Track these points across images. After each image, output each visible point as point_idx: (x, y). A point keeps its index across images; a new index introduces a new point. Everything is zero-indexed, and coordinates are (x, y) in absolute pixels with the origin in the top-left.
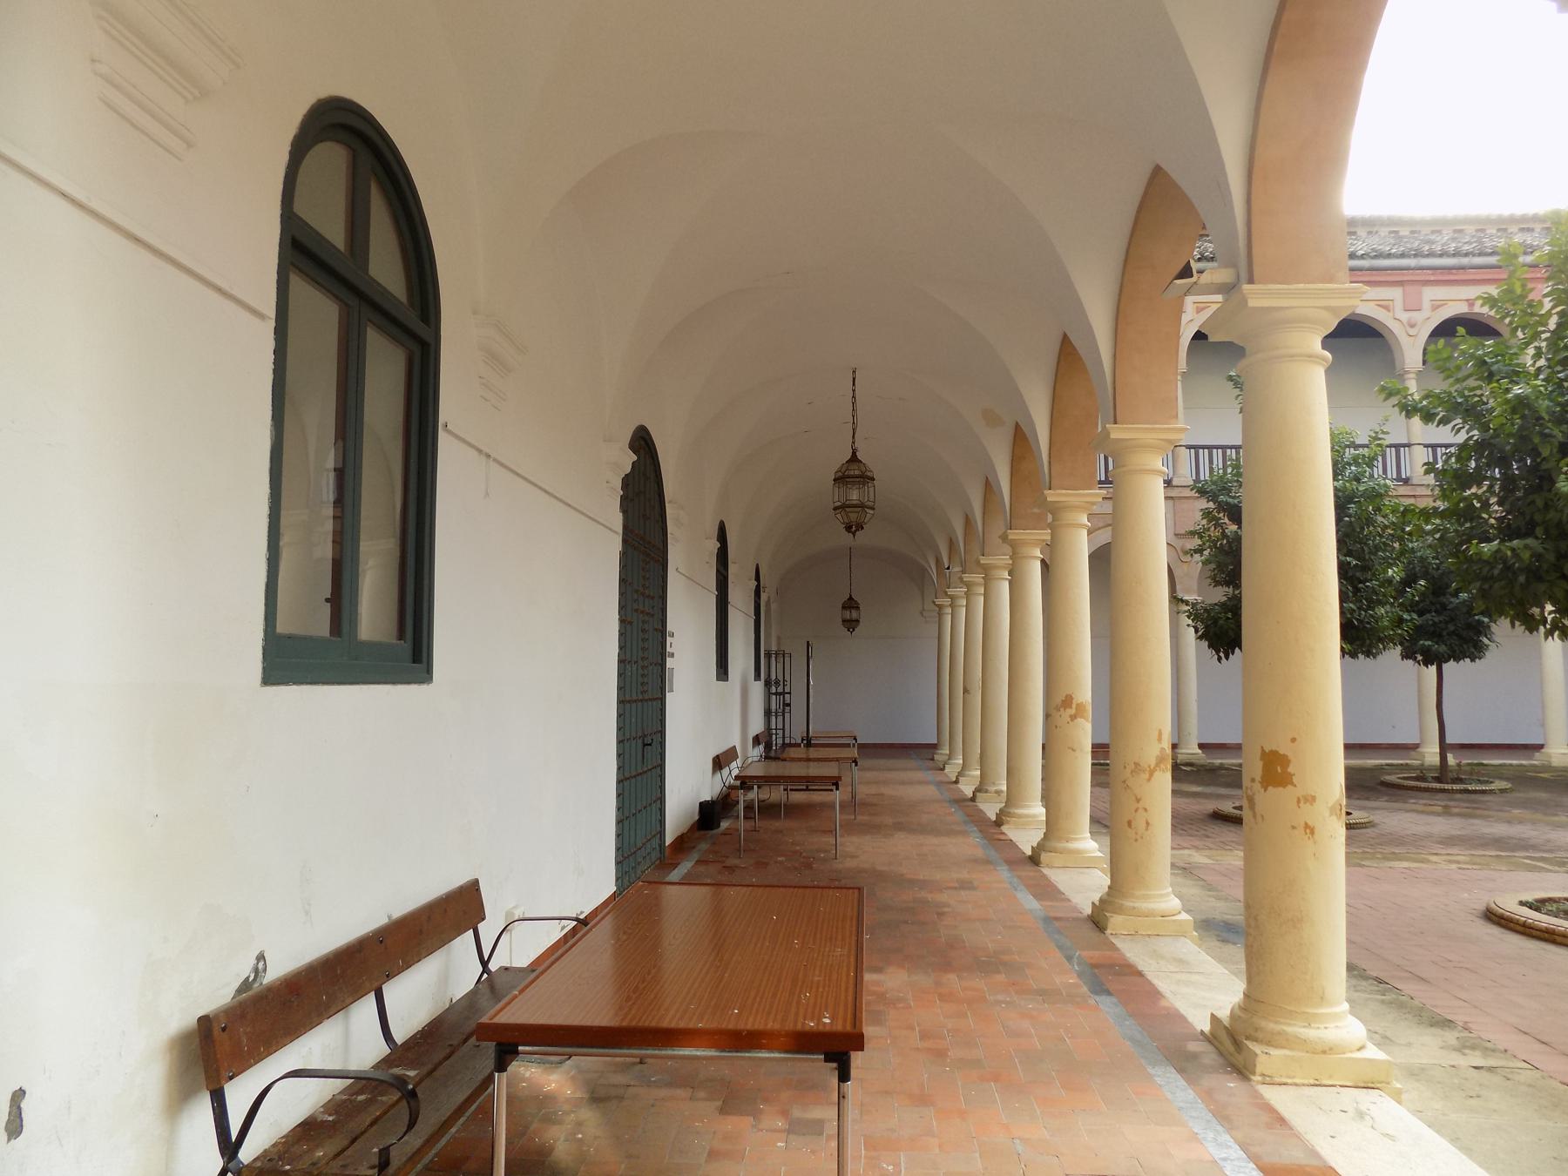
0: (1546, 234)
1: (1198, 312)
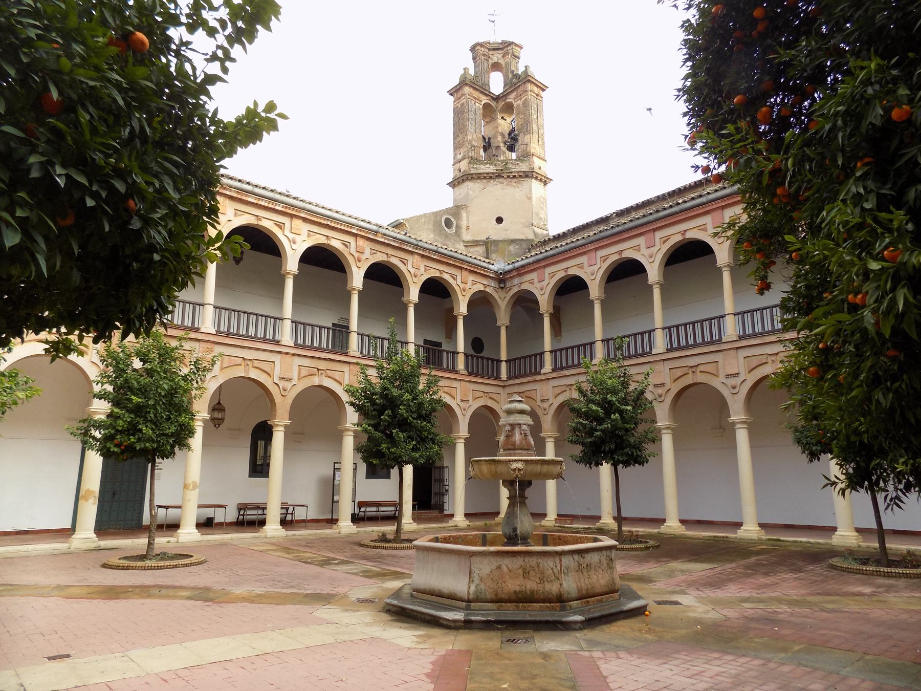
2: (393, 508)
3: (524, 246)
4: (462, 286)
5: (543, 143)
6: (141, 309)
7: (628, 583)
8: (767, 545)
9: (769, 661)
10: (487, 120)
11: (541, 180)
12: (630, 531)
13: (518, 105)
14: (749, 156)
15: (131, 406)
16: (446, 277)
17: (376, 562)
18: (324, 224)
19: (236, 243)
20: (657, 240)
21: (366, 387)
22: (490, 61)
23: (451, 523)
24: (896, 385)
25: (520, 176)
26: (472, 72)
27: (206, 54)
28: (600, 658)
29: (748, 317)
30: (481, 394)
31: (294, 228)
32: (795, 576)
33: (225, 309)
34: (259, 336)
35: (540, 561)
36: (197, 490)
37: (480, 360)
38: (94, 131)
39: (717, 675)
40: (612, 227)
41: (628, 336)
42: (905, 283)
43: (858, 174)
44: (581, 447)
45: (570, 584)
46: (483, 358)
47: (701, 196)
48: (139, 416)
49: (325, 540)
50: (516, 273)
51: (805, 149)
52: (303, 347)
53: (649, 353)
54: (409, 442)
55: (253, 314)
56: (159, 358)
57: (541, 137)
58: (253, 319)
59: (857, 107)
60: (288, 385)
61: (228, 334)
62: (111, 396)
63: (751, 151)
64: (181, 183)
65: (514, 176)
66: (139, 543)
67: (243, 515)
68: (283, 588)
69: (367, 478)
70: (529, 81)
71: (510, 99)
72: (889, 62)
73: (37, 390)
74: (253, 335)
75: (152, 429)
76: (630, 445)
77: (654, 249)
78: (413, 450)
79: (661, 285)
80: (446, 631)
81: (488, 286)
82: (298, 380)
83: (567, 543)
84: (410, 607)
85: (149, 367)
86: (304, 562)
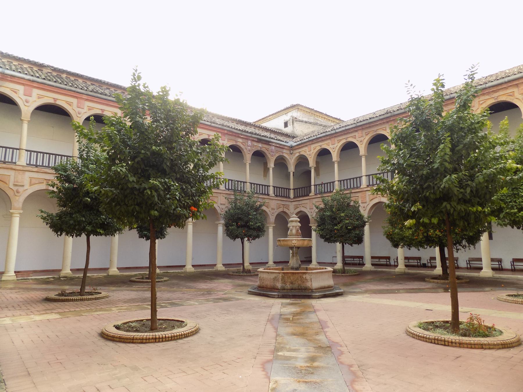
1: (89, 110)
79: (366, 156)
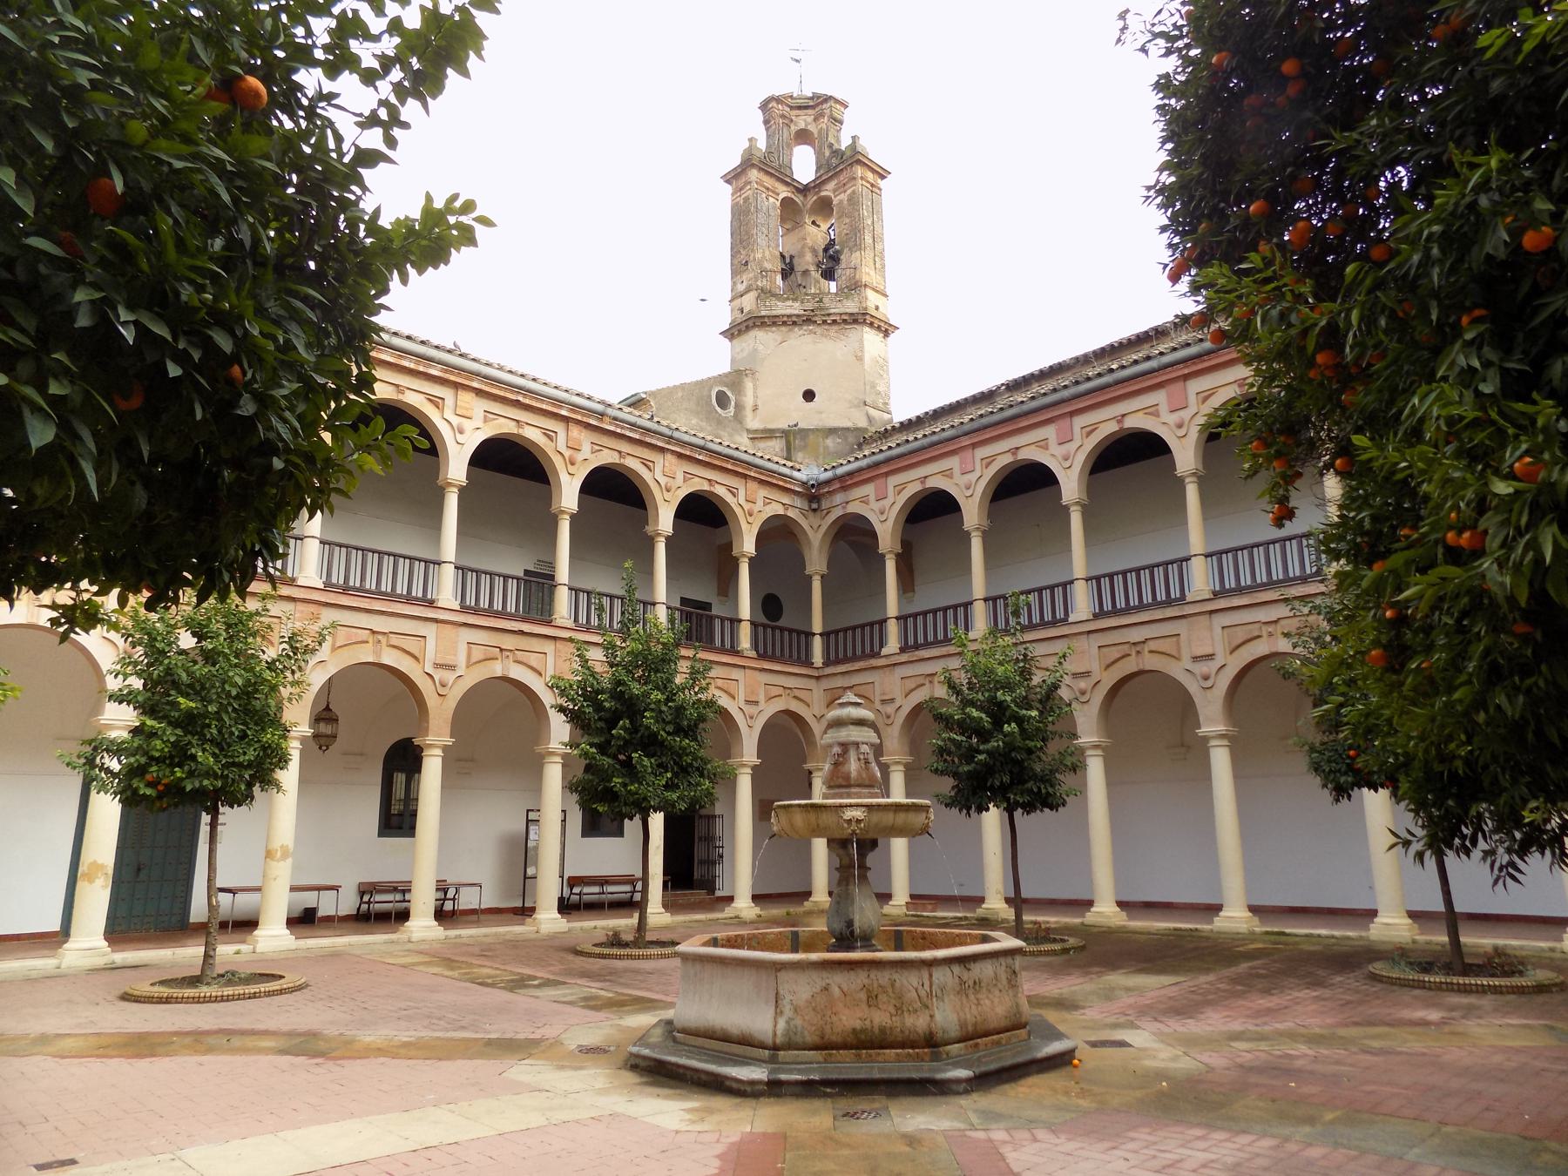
0: (680, 710)
2: (628, 888)
3: (851, 439)
4: (747, 506)
5: (883, 266)
6: (236, 550)
7: (1038, 1011)
8: (1264, 942)
9: (1287, 1139)
10: (788, 226)
11: (879, 328)
12: (1035, 923)
13: (841, 202)
14: (1286, 305)
15: (177, 714)
16: (720, 491)
17: (605, 981)
18: (512, 401)
19: (406, 438)
20: (1077, 429)
21: (585, 680)
22: (793, 127)
23: (729, 912)
24: (1529, 681)
25: (845, 321)
26: (762, 144)
27: (360, 115)
28: (1005, 1142)
29: (1228, 560)
30: (779, 691)
31: (462, 407)
32: (1315, 994)
33: (341, 546)
34: (399, 591)
35: (896, 976)
36: (289, 861)
37: (778, 632)
38: (180, 244)
39: (1204, 1166)
40: (1002, 409)
41: (1028, 592)
42: (1553, 519)
43: (1469, 336)
44: (952, 780)
45: (946, 1016)
46: (782, 629)
47: (1148, 358)
48: (191, 733)
49: (515, 944)
50: (838, 486)
51: (1379, 294)
52: (476, 611)
53: (1065, 620)
54: (661, 774)
55: (389, 554)
56: (226, 630)
57: (879, 256)
58: (388, 562)
59: (1461, 226)
60: (449, 677)
61: (346, 589)
62: (140, 698)
63: (1289, 296)
64: (317, 338)
65: (834, 322)
66: (188, 954)
67: (369, 903)
68: (447, 1030)
69: (583, 836)
70: (859, 162)
71: (827, 191)
72: (1517, 157)
73: (12, 690)
74: (389, 590)
75: (214, 755)
76: (1035, 777)
77: (1072, 446)
78: (667, 787)
79: (1083, 506)
80: (738, 1100)
81: (793, 508)
82: (468, 667)
83: (937, 946)
84: (673, 1059)
85: (210, 647)
86: (480, 984)
